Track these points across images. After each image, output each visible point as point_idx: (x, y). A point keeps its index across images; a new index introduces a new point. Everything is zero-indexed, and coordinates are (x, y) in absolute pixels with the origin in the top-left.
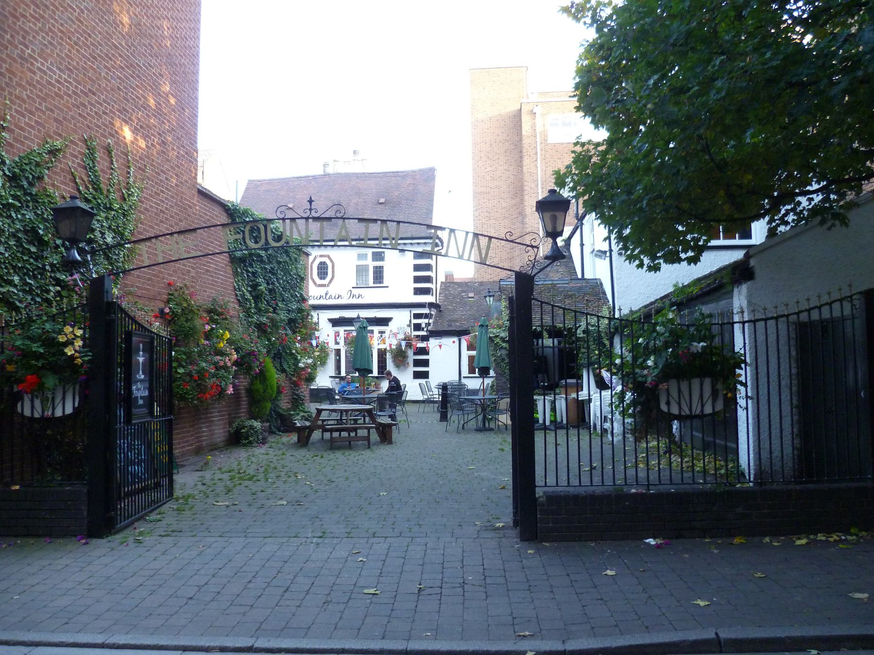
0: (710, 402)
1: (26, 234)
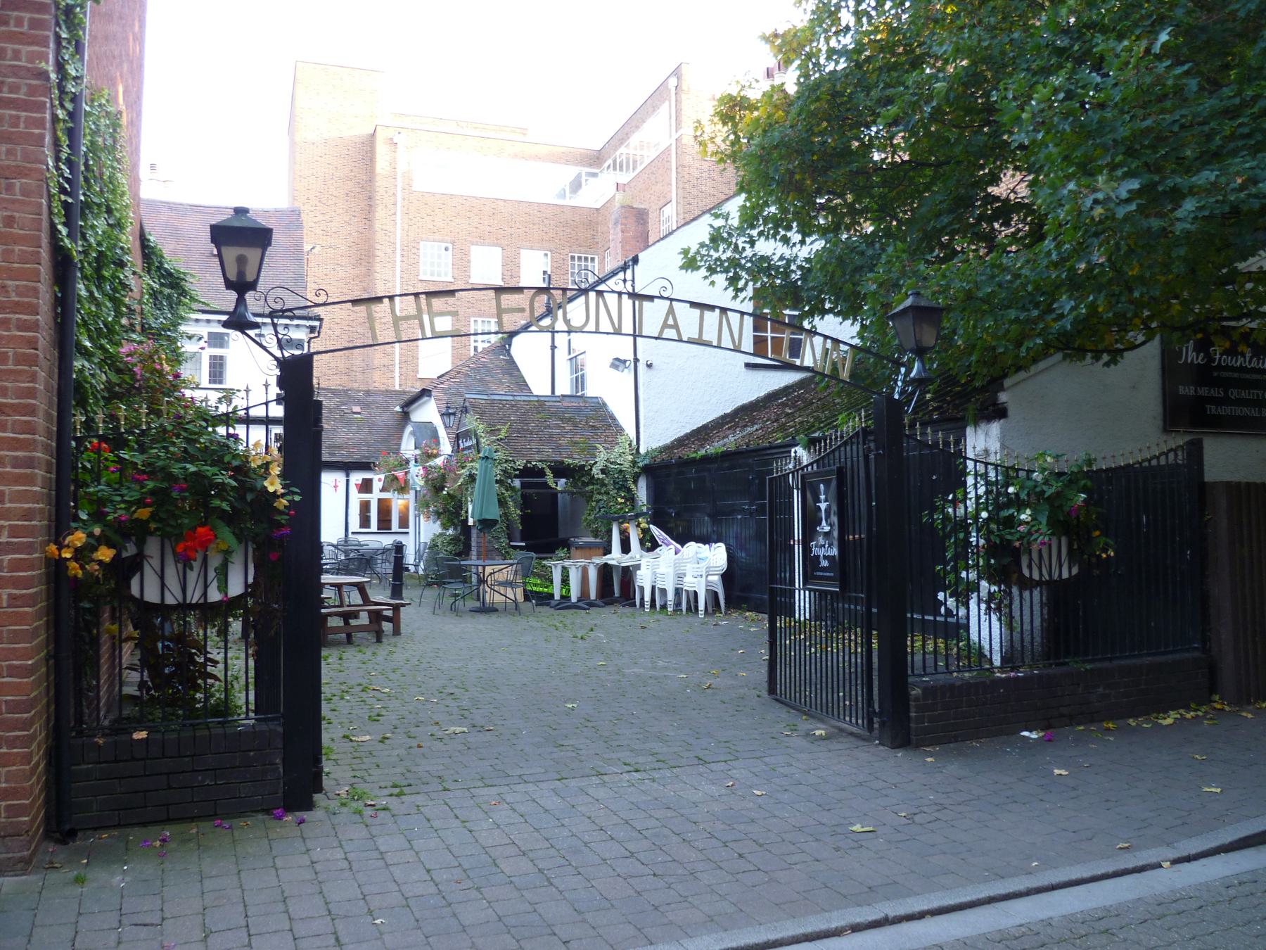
0: (1066, 562)
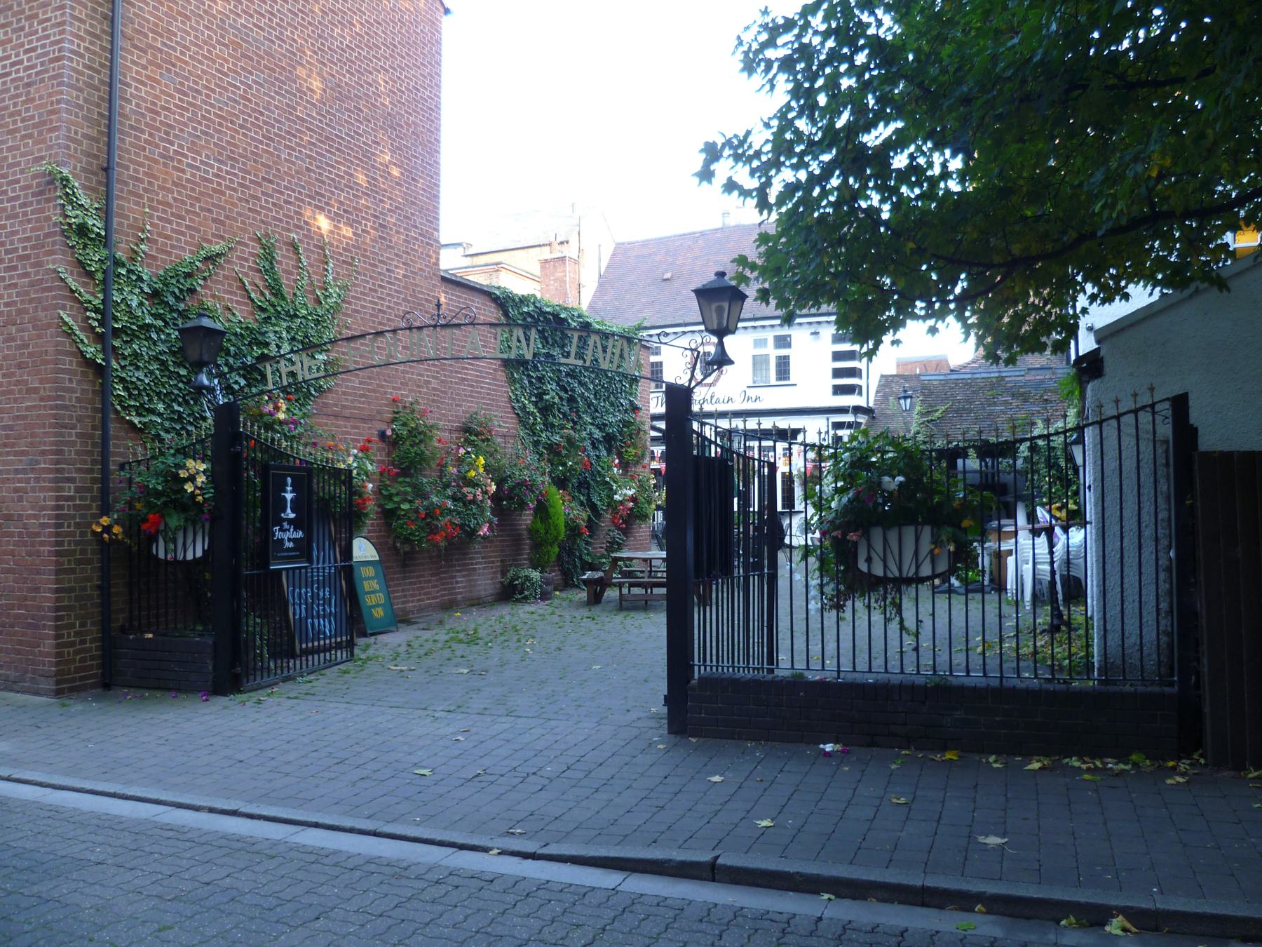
1: (174, 356)
